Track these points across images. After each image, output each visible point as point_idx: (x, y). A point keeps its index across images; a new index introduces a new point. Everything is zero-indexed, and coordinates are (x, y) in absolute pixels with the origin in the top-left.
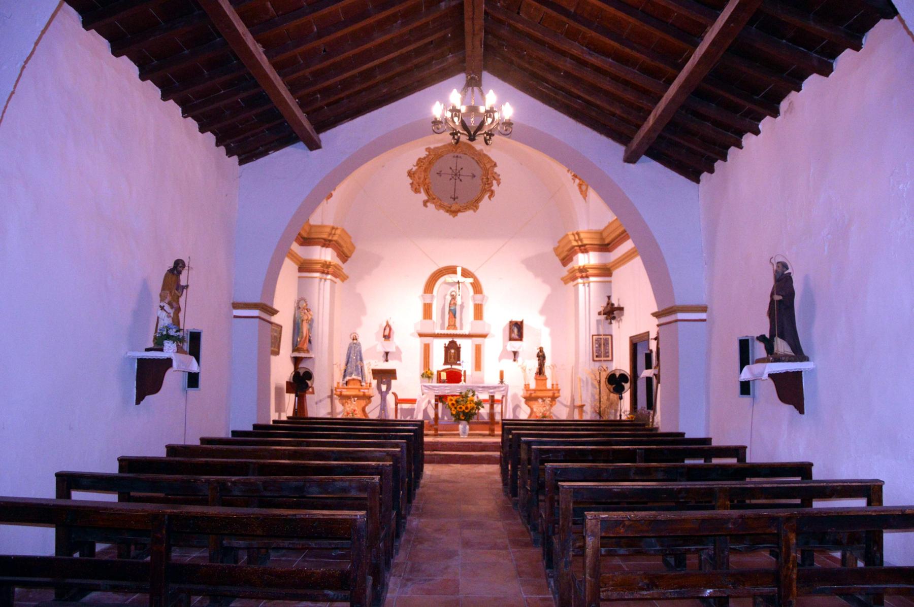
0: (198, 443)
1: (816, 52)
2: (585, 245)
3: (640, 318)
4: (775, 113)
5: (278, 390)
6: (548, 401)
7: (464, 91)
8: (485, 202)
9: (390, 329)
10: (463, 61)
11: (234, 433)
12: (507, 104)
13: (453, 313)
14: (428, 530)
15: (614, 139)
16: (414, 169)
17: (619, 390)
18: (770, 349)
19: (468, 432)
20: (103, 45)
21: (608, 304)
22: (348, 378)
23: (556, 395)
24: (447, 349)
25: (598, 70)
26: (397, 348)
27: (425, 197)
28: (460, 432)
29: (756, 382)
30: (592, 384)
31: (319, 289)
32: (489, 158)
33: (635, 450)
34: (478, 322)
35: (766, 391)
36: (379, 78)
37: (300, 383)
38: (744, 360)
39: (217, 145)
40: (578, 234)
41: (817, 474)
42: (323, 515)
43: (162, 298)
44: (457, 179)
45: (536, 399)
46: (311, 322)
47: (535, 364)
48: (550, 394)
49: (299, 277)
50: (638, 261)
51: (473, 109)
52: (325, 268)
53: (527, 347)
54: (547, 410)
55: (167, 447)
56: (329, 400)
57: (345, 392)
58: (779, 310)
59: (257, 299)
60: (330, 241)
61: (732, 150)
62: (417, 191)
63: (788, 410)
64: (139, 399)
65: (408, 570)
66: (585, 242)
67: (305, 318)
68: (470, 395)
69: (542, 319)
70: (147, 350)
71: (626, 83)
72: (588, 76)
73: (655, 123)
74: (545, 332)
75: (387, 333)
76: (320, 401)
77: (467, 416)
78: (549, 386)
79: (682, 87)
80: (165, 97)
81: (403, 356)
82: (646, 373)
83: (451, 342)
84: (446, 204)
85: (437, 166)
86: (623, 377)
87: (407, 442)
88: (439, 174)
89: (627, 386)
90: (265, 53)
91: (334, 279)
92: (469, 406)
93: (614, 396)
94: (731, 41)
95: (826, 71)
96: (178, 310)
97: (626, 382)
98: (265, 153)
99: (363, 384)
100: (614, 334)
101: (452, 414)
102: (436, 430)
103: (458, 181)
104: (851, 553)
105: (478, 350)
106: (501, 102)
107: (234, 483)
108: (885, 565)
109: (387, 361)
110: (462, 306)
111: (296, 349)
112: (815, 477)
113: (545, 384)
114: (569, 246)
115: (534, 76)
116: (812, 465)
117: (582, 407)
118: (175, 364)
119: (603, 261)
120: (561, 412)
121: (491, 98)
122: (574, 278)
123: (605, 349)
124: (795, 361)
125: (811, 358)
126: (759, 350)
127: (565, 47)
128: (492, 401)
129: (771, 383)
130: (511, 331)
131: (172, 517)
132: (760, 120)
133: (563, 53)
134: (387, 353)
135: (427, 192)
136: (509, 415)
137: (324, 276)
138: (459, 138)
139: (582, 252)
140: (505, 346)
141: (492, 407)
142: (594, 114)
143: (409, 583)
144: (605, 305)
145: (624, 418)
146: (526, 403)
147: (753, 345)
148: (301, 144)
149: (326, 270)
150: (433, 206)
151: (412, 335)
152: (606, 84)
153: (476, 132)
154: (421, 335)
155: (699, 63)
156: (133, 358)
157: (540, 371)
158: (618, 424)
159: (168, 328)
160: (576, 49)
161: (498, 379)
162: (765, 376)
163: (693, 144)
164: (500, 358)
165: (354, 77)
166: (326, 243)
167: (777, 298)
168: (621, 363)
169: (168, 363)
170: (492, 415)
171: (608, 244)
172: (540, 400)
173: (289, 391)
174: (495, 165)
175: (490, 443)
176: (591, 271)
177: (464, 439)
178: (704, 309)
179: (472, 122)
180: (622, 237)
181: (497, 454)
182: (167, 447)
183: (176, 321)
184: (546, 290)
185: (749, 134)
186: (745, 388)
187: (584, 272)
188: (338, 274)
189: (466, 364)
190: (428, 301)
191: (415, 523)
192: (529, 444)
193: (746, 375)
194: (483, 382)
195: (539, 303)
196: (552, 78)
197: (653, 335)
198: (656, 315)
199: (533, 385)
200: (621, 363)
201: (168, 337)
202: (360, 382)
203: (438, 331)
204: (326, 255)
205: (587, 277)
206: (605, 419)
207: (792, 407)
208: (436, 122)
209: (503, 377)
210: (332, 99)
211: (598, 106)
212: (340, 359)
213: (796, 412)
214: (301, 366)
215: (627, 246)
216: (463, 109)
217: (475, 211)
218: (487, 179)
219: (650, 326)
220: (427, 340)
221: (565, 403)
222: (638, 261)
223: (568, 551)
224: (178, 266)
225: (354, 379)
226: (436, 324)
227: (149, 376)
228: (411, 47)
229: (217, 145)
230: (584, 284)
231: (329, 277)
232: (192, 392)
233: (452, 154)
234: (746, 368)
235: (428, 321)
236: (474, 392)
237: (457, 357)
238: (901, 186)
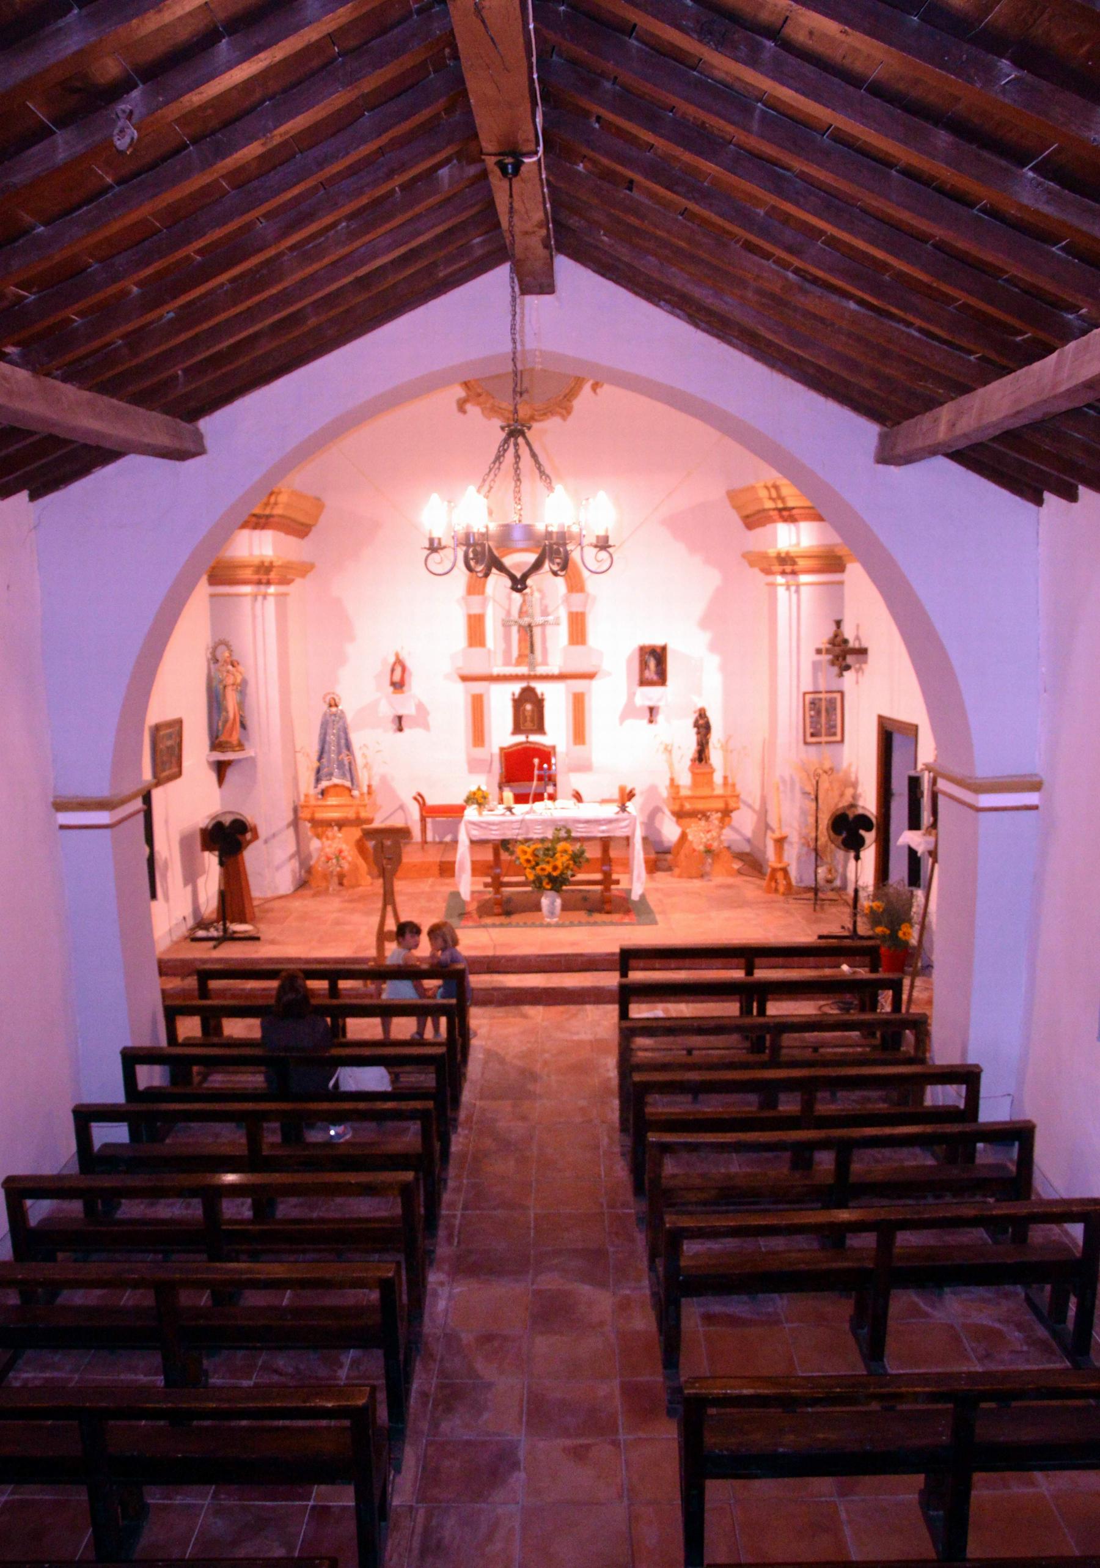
5: (185, 842)
6: (715, 817)
9: (404, 669)
17: (855, 845)
21: (836, 636)
22: (324, 784)
23: (732, 805)
24: (518, 703)
31: (254, 617)
34: (578, 648)
44: (521, 405)
45: (693, 814)
46: (242, 688)
48: (720, 805)
49: (212, 596)
52: (264, 574)
54: (713, 839)
56: (291, 830)
57: (321, 815)
60: (268, 517)
67: (230, 680)
69: (705, 637)
74: (712, 663)
75: (397, 677)
76: (274, 835)
81: (431, 719)
86: (864, 822)
89: (870, 837)
92: (559, 864)
97: (869, 829)
105: (579, 703)
109: (400, 729)
111: (216, 744)
113: (710, 783)
130: (644, 665)
134: (400, 718)
137: (263, 588)
139: (785, 520)
140: (631, 695)
149: (264, 578)
154: (465, 679)
157: (701, 755)
176: (802, 563)
178: (1036, 786)
184: (713, 578)
187: (787, 563)
190: (476, 610)
195: (699, 608)
202: (350, 790)
203: (497, 670)
205: (794, 573)
212: (308, 742)
217: (564, 418)
220: (477, 687)
225: (336, 786)
230: (788, 587)
231: (272, 589)
235: (477, 651)
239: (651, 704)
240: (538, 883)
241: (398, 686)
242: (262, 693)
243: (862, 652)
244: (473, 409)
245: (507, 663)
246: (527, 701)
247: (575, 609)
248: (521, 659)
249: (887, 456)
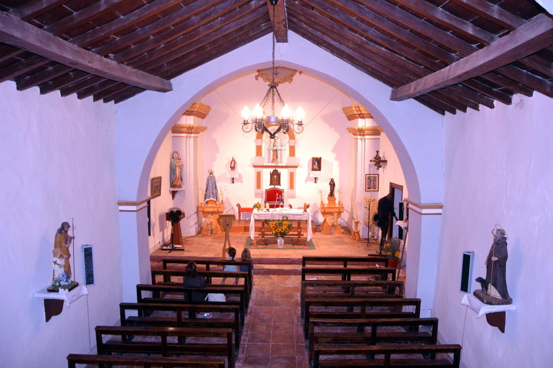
5: (161, 217)
6: (336, 214)
9: (235, 163)
22: (207, 200)
24: (272, 175)
26: (240, 175)
31: (186, 144)
34: (293, 158)
46: (181, 167)
47: (327, 189)
48: (338, 210)
53: (324, 175)
57: (206, 210)
60: (192, 111)
66: (363, 112)
69: (334, 155)
74: (336, 164)
81: (243, 180)
83: (274, 171)
99: (217, 203)
100: (380, 174)
105: (292, 176)
109: (233, 182)
111: (172, 186)
113: (334, 203)
123: (374, 184)
125: (514, 302)
130: (313, 164)
134: (233, 179)
137: (190, 135)
139: (361, 118)
140: (309, 174)
149: (190, 131)
150: (262, 79)
151: (249, 166)
154: (255, 166)
157: (332, 194)
164: (306, 181)
167: (494, 259)
176: (366, 132)
178: (441, 207)
184: (337, 136)
187: (361, 132)
212: (203, 186)
217: (290, 83)
220: (259, 169)
224: (64, 228)
231: (193, 135)
235: (259, 157)
240: (276, 235)
241: (233, 168)
243: (385, 161)
247: (291, 145)
248: (274, 160)
249: (395, 97)
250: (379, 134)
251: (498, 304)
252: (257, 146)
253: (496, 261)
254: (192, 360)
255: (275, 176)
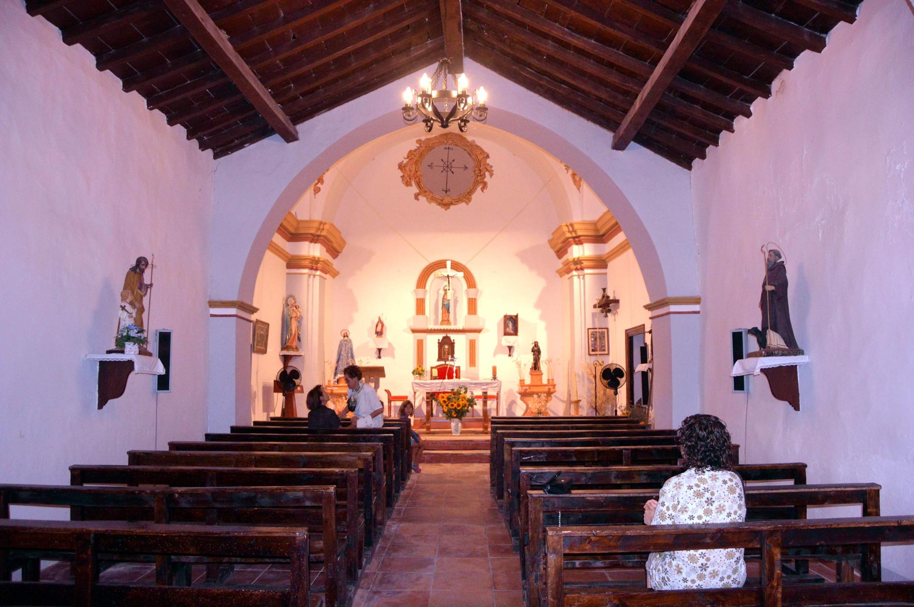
0: (167, 448)
1: (807, 27)
2: (579, 237)
3: (633, 313)
4: (767, 94)
5: (265, 389)
6: (543, 396)
7: (436, 76)
8: (478, 194)
10: (442, 47)
11: (208, 436)
12: (482, 88)
13: (446, 308)
14: (405, 535)
15: (601, 125)
16: (405, 161)
17: (614, 385)
18: (762, 342)
19: (460, 428)
20: (54, 32)
21: (603, 297)
24: (441, 345)
25: (579, 51)
26: (390, 344)
27: (417, 191)
28: (453, 429)
29: (751, 377)
30: (588, 379)
31: (308, 285)
32: (481, 149)
33: (621, 451)
34: (473, 316)
35: (759, 386)
36: (354, 65)
37: (287, 381)
38: (738, 354)
39: (188, 138)
40: (572, 225)
41: (813, 478)
42: (259, 533)
43: (123, 299)
44: (447, 170)
45: (531, 394)
46: (299, 320)
47: (530, 358)
48: (546, 389)
50: (630, 253)
51: (445, 94)
52: (314, 264)
53: (522, 342)
55: (129, 453)
58: (771, 301)
59: (234, 297)
60: (318, 236)
61: (724, 134)
62: (408, 184)
63: (784, 406)
64: (102, 404)
65: (377, 581)
66: (579, 233)
67: (294, 315)
68: (463, 391)
69: (538, 312)
70: (109, 352)
71: (611, 65)
72: (570, 57)
73: (641, 107)
74: (542, 325)
75: (379, 329)
77: (460, 414)
78: (545, 381)
79: (667, 68)
80: (127, 88)
82: (640, 367)
83: (444, 338)
84: (437, 197)
85: (428, 158)
86: (618, 372)
87: (398, 443)
88: (430, 166)
89: (623, 380)
90: (229, 40)
91: (324, 275)
92: (461, 403)
93: (610, 392)
94: (716, 16)
95: (818, 46)
96: (141, 310)
97: (622, 376)
98: (240, 146)
101: (444, 412)
102: (428, 428)
103: (450, 173)
104: (847, 563)
105: (472, 345)
106: (475, 86)
107: (180, 494)
108: (885, 578)
109: (380, 357)
110: (456, 301)
111: (284, 347)
112: (809, 482)
114: (563, 239)
115: (517, 60)
116: (806, 466)
117: (578, 402)
118: (136, 366)
119: (598, 253)
120: (557, 408)
121: (463, 82)
122: (569, 271)
124: (788, 354)
125: (805, 352)
126: (751, 344)
127: (545, 29)
128: (485, 397)
129: (764, 378)
130: (506, 326)
131: (99, 535)
132: (751, 103)
133: (546, 36)
134: (380, 350)
135: (418, 185)
136: (503, 413)
137: (313, 272)
138: (432, 125)
140: (500, 341)
141: (485, 403)
142: (580, 99)
143: (376, 597)
144: (600, 297)
145: (619, 413)
146: (521, 399)
147: (747, 340)
148: (277, 136)
150: (425, 199)
151: (405, 331)
152: (590, 67)
153: (448, 119)
154: (414, 331)
155: (683, 41)
156: (94, 360)
157: (536, 366)
158: (614, 421)
159: (128, 329)
160: (557, 30)
161: (491, 376)
162: (758, 371)
163: (683, 129)
164: (495, 354)
165: (327, 64)
166: (314, 239)
167: (769, 288)
168: (617, 357)
169: (130, 365)
170: (485, 412)
171: (603, 235)
172: (535, 396)
173: (276, 390)
174: (488, 156)
175: (482, 441)
176: (585, 263)
177: (457, 437)
178: (697, 301)
179: (445, 108)
180: (615, 229)
181: (488, 452)
182: (129, 453)
183: (139, 324)
185: (740, 117)
186: (739, 383)
187: (578, 264)
188: (327, 269)
189: (460, 359)
190: (421, 296)
191: (394, 528)
192: (513, 444)
193: (738, 369)
194: (478, 379)
196: (534, 61)
197: (647, 329)
198: (649, 307)
199: (528, 381)
200: (617, 357)
201: (129, 338)
204: (315, 250)
205: (582, 269)
206: (601, 415)
207: (787, 403)
208: (407, 109)
209: (498, 374)
210: (307, 88)
211: (583, 91)
213: (791, 408)
214: (290, 364)
215: (620, 238)
216: (435, 94)
218: (479, 169)
219: (643, 318)
220: (420, 336)
221: (562, 398)
222: (630, 253)
223: (539, 565)
224: (141, 265)
226: (430, 320)
227: (112, 380)
228: (387, 32)
229: (188, 138)
230: (579, 276)
231: (318, 273)
232: (162, 393)
233: (443, 146)
234: (737, 362)
236: (466, 389)
237: (452, 352)
238: (898, 168)
239: (510, 345)
241: (379, 334)
242: (310, 326)
243: (617, 301)
244: (422, 199)
245: (436, 323)
246: (445, 344)
250: (605, 267)
251: (782, 355)
252: (418, 300)
253: (773, 291)
254: (357, 52)
255: (446, 347)
